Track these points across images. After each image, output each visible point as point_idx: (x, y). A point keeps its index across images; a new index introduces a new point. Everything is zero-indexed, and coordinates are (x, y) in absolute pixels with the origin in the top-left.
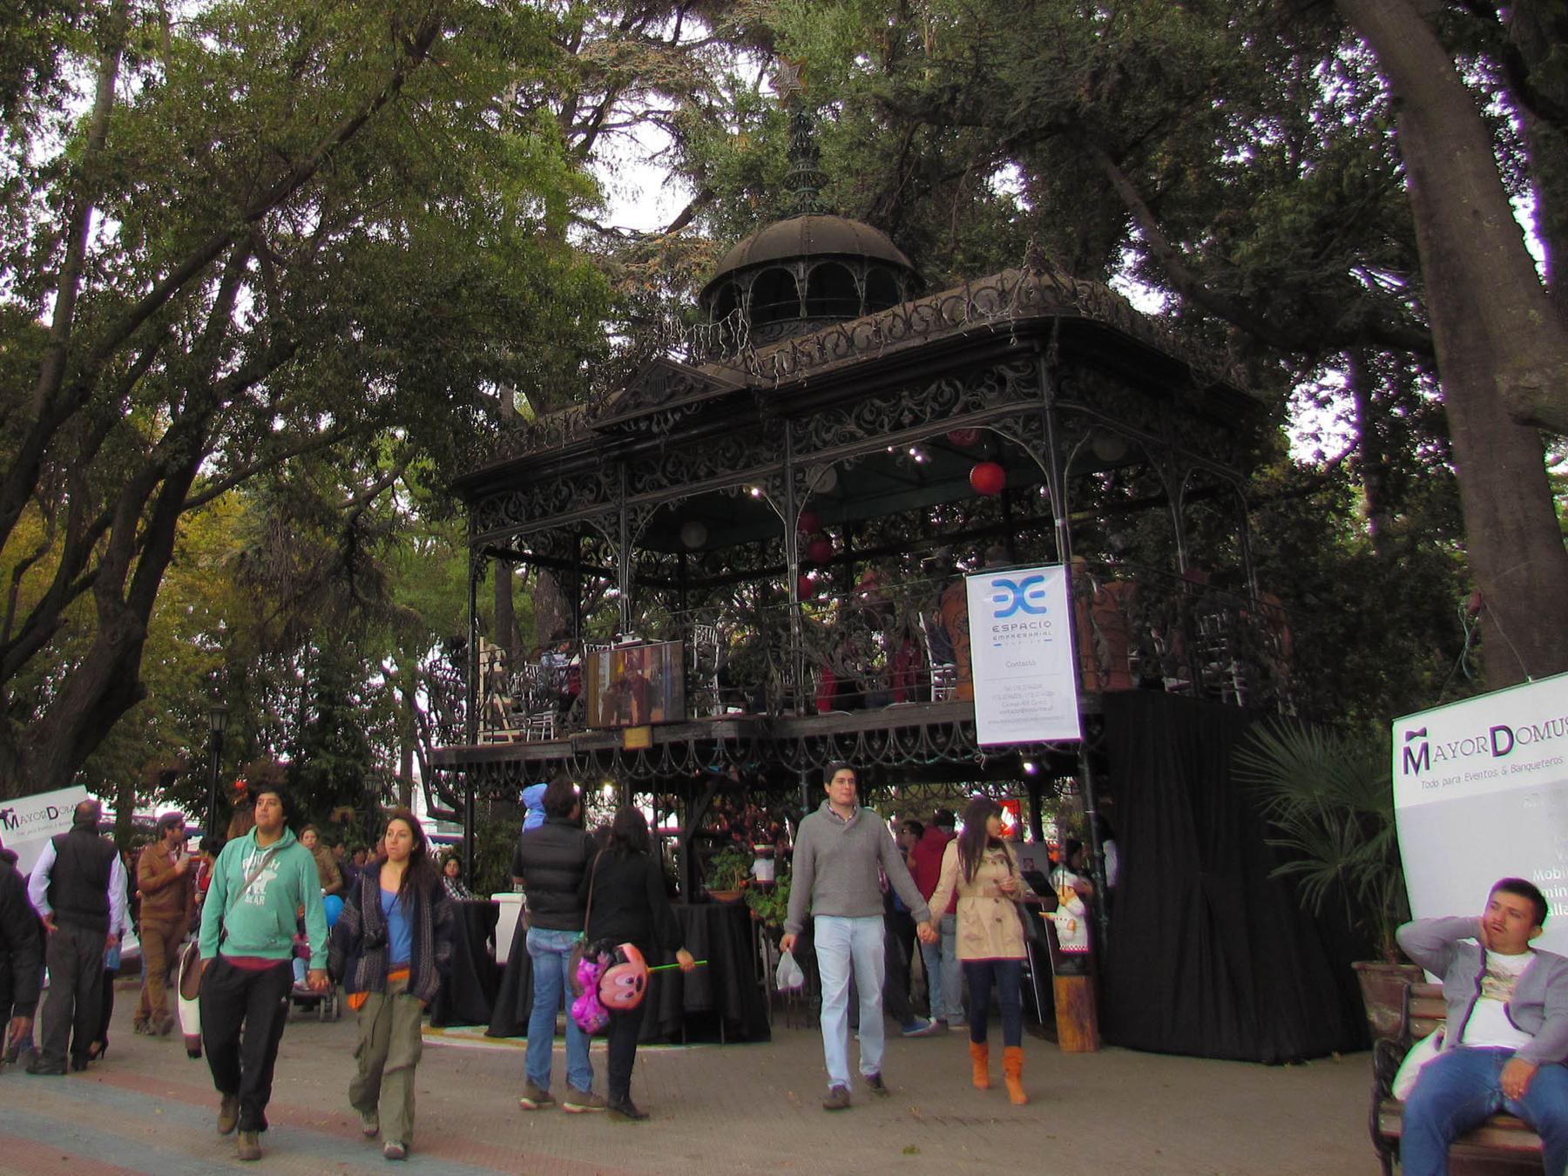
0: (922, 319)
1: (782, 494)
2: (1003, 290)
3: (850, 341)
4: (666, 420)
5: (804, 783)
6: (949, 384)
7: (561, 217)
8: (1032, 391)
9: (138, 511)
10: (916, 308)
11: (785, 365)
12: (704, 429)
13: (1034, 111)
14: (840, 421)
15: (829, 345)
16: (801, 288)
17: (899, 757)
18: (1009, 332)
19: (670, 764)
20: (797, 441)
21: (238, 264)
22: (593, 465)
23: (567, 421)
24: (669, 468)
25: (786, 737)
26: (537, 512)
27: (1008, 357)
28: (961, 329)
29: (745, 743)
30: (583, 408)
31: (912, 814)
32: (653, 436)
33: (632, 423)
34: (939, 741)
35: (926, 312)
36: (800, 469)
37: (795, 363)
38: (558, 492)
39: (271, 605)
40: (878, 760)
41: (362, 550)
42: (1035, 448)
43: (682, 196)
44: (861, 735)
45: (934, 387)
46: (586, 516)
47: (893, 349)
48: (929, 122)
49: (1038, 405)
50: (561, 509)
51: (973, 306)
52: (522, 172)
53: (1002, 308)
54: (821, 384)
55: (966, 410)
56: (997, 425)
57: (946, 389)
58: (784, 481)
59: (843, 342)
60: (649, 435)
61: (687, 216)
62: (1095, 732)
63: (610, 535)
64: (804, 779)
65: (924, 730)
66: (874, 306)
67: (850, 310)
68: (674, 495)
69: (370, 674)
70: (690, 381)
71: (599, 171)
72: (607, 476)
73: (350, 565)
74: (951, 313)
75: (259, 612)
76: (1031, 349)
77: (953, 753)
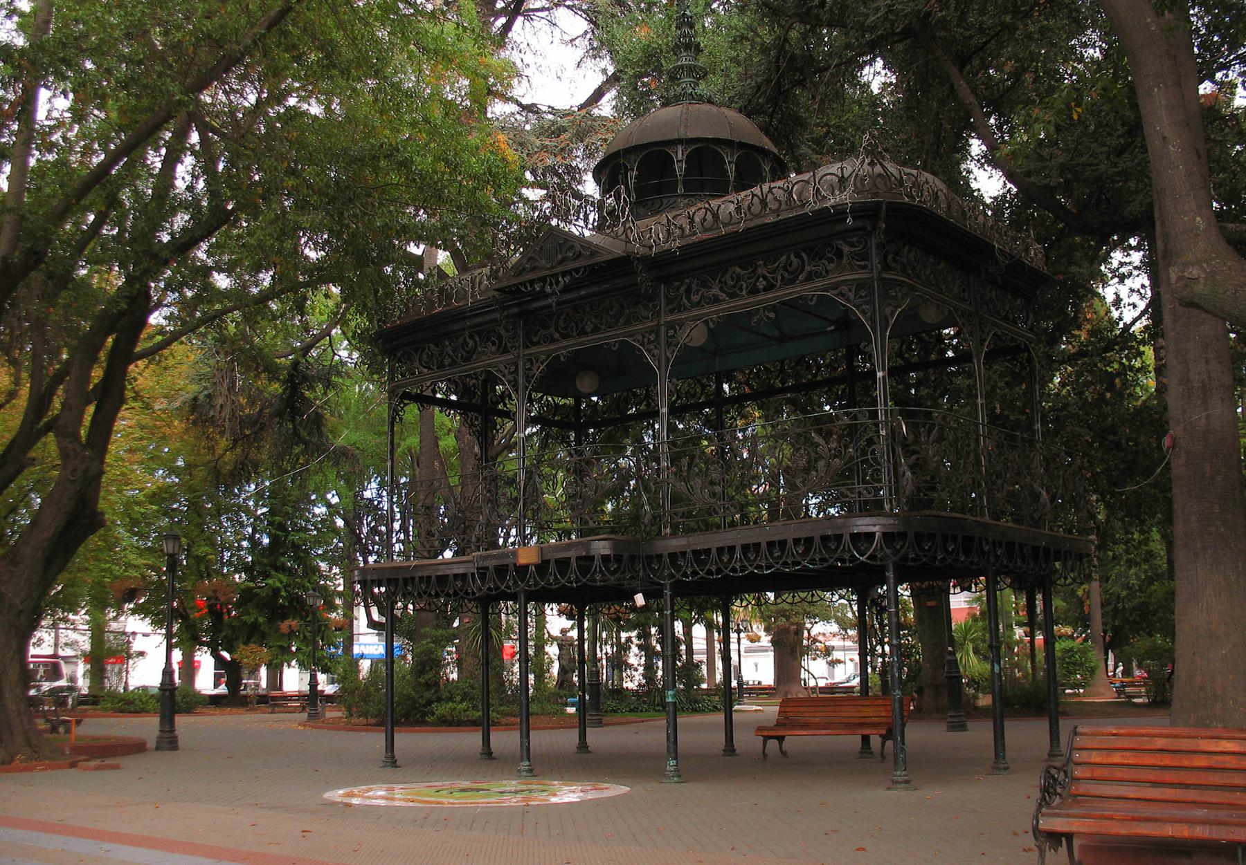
0: (775, 199)
1: (656, 348)
2: (843, 177)
3: (715, 216)
4: (558, 282)
5: (668, 592)
6: (798, 256)
7: (484, 93)
8: (862, 263)
9: (95, 360)
10: (771, 189)
11: (661, 236)
12: (595, 289)
13: (891, 17)
14: (706, 285)
15: (697, 219)
16: (680, 168)
17: (743, 568)
18: (846, 213)
19: (495, 583)
20: (669, 301)
21: (182, 135)
22: (495, 320)
23: (473, 282)
24: (561, 324)
25: (654, 554)
26: (447, 361)
27: (845, 234)
28: (807, 209)
29: (618, 558)
30: (487, 271)
31: (784, 620)
32: (547, 296)
33: (528, 284)
34: (776, 555)
35: (779, 193)
36: (670, 326)
37: (669, 234)
38: (465, 343)
39: (223, 443)
40: (727, 571)
41: (303, 394)
42: (863, 312)
43: (592, 76)
44: (714, 551)
45: (784, 258)
46: (489, 365)
47: (752, 224)
48: (803, 22)
49: (866, 276)
50: (467, 359)
51: (818, 189)
52: (443, 56)
53: (841, 192)
54: (692, 252)
55: (809, 279)
56: (834, 292)
57: (795, 261)
58: (658, 336)
59: (709, 216)
60: (543, 295)
61: (598, 95)
62: (898, 547)
63: (509, 382)
64: (668, 587)
65: (764, 546)
66: (740, 187)
67: (720, 189)
68: (564, 347)
69: (314, 503)
70: (578, 248)
71: (515, 57)
72: (507, 330)
73: (293, 408)
74: (800, 194)
75: (211, 449)
76: (864, 228)
77: (785, 563)
